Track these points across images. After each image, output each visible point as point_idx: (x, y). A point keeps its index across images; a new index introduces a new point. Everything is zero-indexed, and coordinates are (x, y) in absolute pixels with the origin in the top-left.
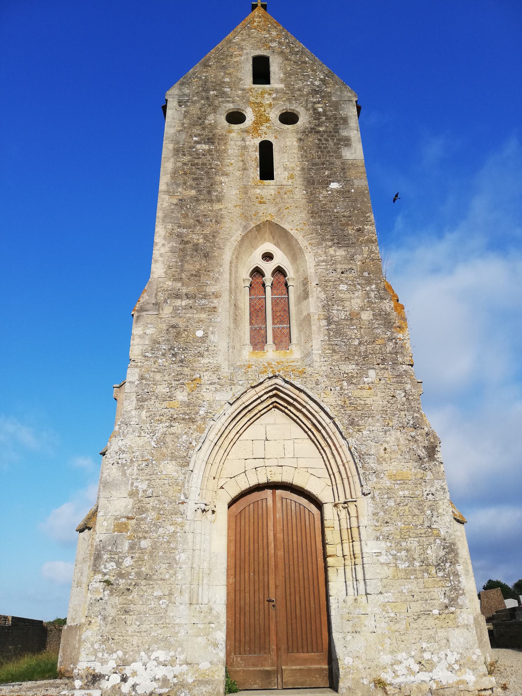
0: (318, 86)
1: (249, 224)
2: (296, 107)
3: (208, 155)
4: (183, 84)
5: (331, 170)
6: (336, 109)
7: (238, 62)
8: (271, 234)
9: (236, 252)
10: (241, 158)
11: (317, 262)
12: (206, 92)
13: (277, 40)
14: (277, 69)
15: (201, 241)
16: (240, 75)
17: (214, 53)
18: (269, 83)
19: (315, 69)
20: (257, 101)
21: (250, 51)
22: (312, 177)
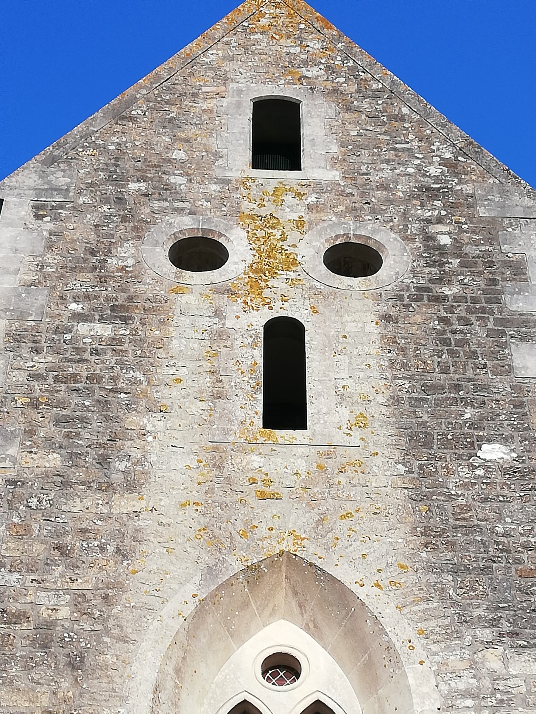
0: (437, 179)
1: (224, 561)
2: (374, 231)
3: (110, 353)
4: (53, 161)
5: (480, 408)
6: (491, 239)
7: (211, 111)
8: (296, 593)
9: (177, 653)
10: (207, 366)
11: (446, 697)
12: (116, 185)
13: (323, 61)
14: (322, 133)
15: (64, 612)
16: (214, 144)
17: (145, 87)
18: (296, 165)
19: (429, 136)
20: (263, 212)
21: (247, 87)
22: (424, 424)
